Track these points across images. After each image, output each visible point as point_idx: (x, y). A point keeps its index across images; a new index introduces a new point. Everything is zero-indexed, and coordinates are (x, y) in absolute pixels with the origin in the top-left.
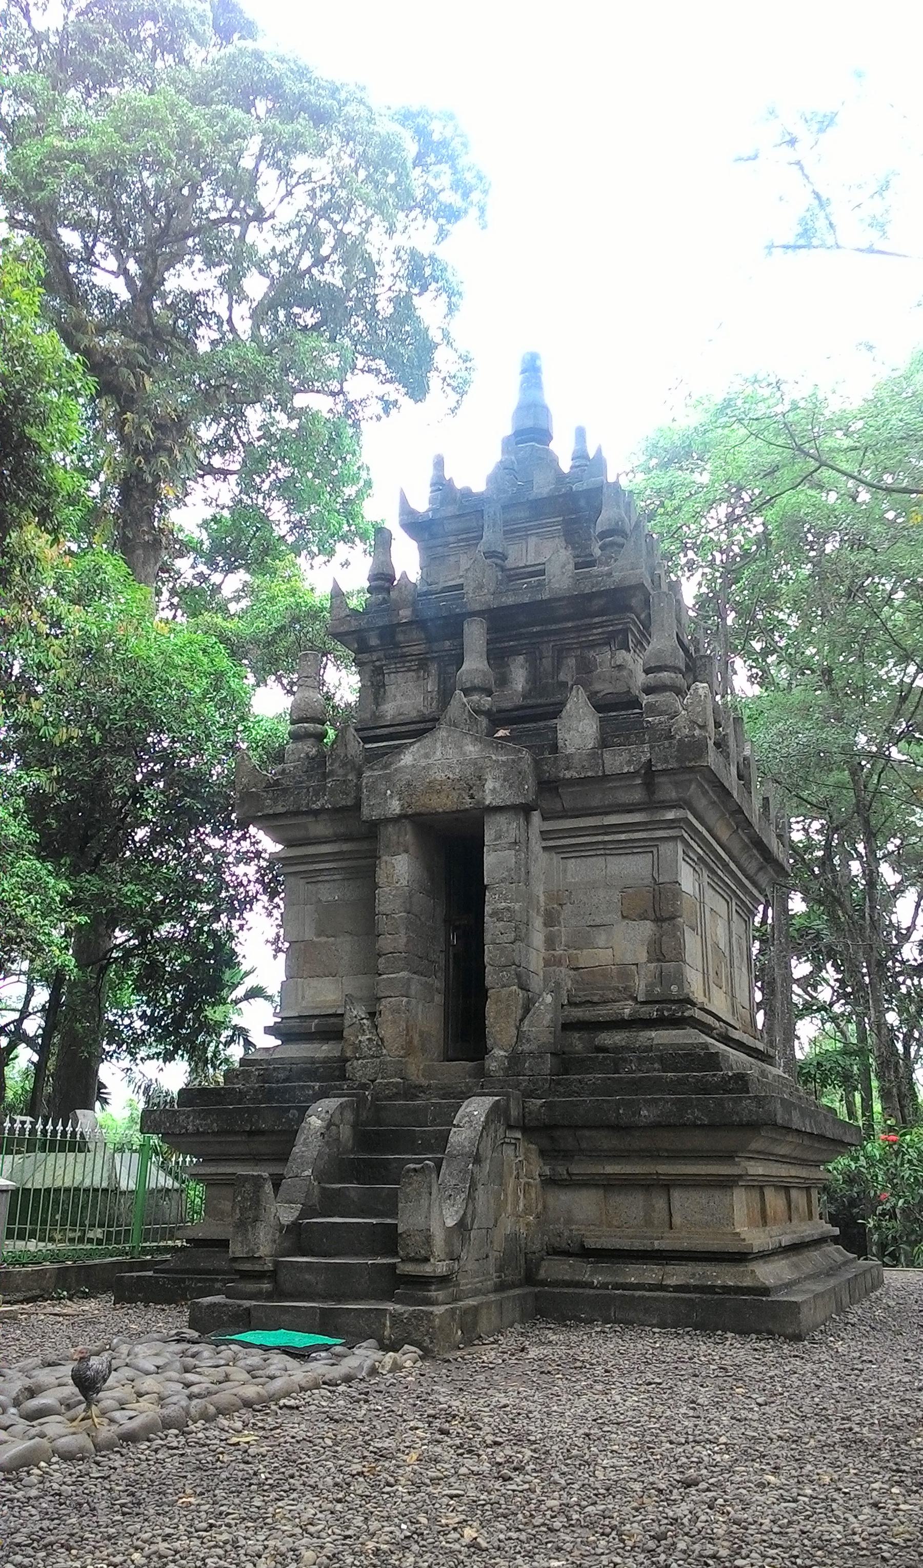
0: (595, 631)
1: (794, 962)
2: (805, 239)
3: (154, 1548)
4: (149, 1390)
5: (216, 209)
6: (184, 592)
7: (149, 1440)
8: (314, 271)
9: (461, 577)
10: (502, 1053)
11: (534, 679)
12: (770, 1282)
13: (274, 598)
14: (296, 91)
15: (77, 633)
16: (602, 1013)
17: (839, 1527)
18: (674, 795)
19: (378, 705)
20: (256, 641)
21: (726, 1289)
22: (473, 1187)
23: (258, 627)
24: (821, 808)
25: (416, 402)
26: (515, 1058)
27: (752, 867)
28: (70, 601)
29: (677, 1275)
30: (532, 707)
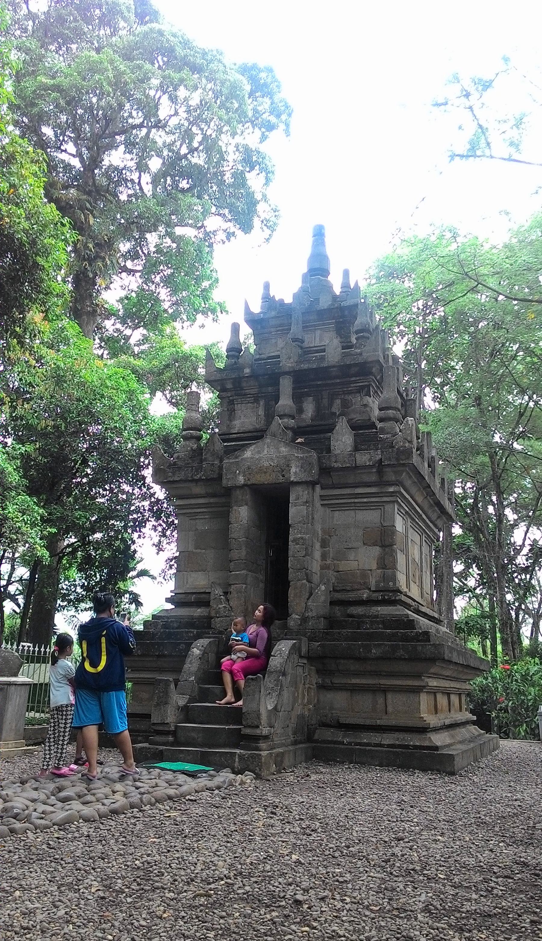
0: (352, 385)
1: (454, 563)
2: (472, 152)
3: (144, 859)
4: (118, 789)
5: (132, 117)
6: (108, 340)
7: (124, 813)
8: (189, 156)
9: (278, 351)
10: (297, 617)
11: (318, 409)
12: (439, 744)
13: (163, 348)
14: (182, 54)
15: (53, 366)
16: (352, 596)
17: (474, 859)
18: (393, 478)
19: (231, 421)
20: (151, 372)
21: (416, 747)
22: (281, 690)
23: (154, 364)
24: (473, 477)
25: (246, 234)
26: (304, 620)
27: (434, 517)
28: (47, 347)
29: (388, 739)
30: (316, 426)
